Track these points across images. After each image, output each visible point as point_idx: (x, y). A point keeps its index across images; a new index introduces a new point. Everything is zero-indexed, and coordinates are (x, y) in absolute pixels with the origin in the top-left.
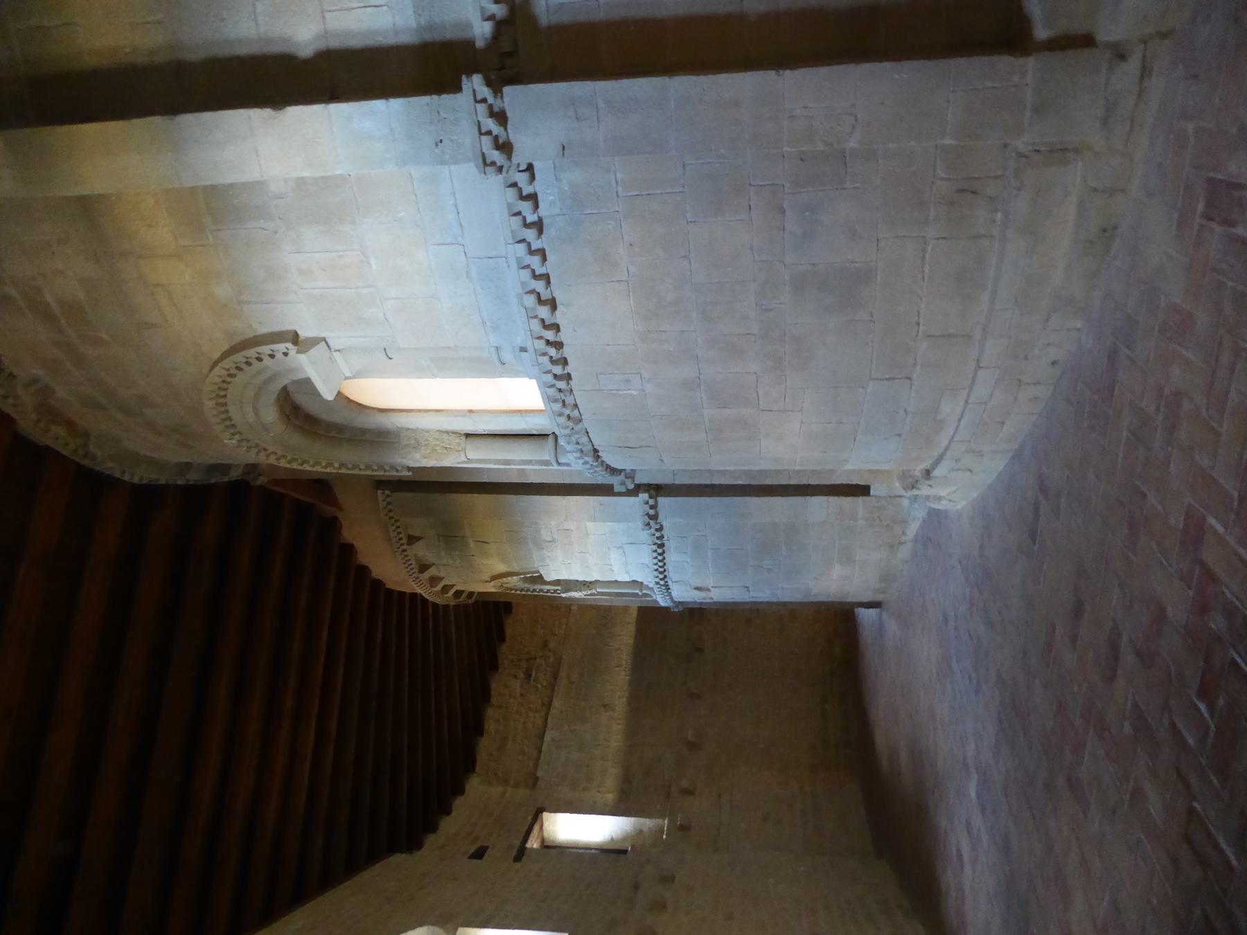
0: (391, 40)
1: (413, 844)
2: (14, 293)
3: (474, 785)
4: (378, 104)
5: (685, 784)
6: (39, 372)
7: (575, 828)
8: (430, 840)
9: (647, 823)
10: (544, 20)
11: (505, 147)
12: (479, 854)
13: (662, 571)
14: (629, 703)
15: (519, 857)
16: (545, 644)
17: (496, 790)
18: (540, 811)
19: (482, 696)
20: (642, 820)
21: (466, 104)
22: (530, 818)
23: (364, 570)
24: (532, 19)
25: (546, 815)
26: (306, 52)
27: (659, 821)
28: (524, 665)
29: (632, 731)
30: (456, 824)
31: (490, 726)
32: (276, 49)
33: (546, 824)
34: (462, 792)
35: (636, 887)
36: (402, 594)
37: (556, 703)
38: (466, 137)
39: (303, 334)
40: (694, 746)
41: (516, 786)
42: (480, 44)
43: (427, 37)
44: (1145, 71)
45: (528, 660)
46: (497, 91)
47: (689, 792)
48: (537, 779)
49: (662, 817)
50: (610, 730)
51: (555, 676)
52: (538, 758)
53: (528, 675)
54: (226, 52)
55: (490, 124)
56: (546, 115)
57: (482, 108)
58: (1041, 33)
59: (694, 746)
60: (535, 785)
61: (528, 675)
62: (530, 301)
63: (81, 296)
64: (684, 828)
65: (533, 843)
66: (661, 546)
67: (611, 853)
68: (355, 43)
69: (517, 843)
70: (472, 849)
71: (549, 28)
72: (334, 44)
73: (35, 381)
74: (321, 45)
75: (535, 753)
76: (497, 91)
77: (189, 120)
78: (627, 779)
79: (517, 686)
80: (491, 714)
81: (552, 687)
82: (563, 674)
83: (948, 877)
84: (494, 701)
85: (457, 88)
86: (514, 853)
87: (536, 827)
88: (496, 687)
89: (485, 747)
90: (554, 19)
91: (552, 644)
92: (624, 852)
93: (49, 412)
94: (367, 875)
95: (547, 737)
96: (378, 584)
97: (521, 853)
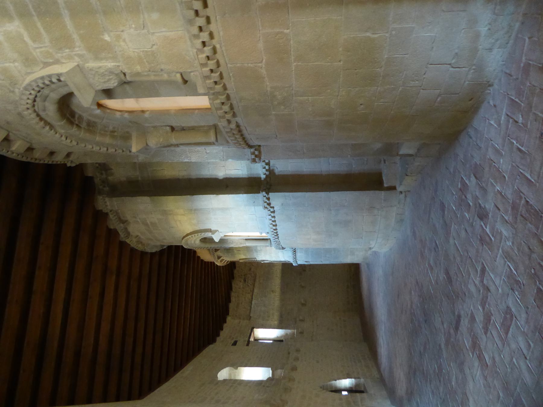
0: (241, 176)
1: (213, 341)
2: (139, 220)
3: (229, 319)
4: (241, 195)
5: (301, 318)
6: (139, 234)
7: (266, 334)
8: (218, 339)
9: (289, 331)
10: (277, 174)
11: (269, 204)
12: (235, 344)
13: (295, 258)
14: (281, 290)
15: (248, 345)
16: (250, 269)
17: (237, 321)
18: (253, 328)
19: (229, 288)
20: (287, 330)
21: (260, 197)
22: (250, 331)
23: (199, 257)
24: (274, 173)
25: (255, 329)
26: (221, 178)
27: (293, 330)
28: (243, 277)
29: (282, 300)
30: (225, 333)
31: (233, 299)
32: (214, 177)
33: (255, 333)
34: (226, 322)
35: (289, 353)
36: (208, 262)
37: (255, 291)
38: (261, 202)
39: (213, 229)
40: (303, 305)
41: (244, 319)
42: (262, 179)
43: (250, 176)
44: (406, 196)
45: (244, 275)
46: (268, 194)
47: (302, 321)
48: (251, 317)
49: (294, 329)
50: (275, 299)
51: (255, 281)
52: (251, 310)
53: (245, 281)
54: (201, 177)
55: (267, 200)
56: (278, 199)
57: (265, 198)
58: (385, 185)
59: (303, 305)
60: (250, 319)
61: (245, 281)
62: (271, 226)
63: (157, 222)
64: (302, 333)
65: (252, 339)
66: (295, 251)
67: (278, 341)
68: (233, 177)
69: (247, 339)
70: (233, 342)
71: (279, 175)
72: (228, 176)
73: (137, 236)
74: (225, 177)
75: (249, 308)
76: (268, 194)
77: (196, 197)
78: (281, 316)
79: (241, 285)
80: (233, 294)
81: (254, 285)
82: (257, 280)
83: (379, 350)
84: (233, 290)
85: (260, 193)
86: (246, 343)
87: (252, 334)
88: (234, 285)
89: (232, 306)
90: (279, 173)
91: (252, 270)
92: (282, 341)
93: (139, 242)
94: (205, 352)
95: (253, 303)
96: (202, 260)
97: (249, 341)
